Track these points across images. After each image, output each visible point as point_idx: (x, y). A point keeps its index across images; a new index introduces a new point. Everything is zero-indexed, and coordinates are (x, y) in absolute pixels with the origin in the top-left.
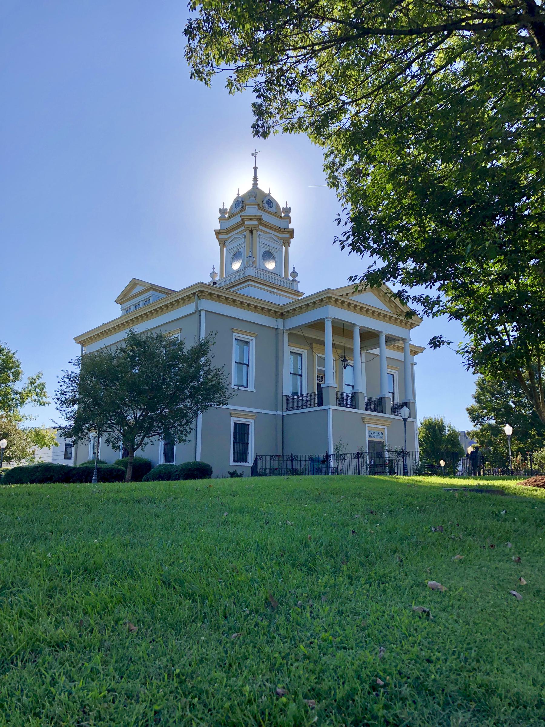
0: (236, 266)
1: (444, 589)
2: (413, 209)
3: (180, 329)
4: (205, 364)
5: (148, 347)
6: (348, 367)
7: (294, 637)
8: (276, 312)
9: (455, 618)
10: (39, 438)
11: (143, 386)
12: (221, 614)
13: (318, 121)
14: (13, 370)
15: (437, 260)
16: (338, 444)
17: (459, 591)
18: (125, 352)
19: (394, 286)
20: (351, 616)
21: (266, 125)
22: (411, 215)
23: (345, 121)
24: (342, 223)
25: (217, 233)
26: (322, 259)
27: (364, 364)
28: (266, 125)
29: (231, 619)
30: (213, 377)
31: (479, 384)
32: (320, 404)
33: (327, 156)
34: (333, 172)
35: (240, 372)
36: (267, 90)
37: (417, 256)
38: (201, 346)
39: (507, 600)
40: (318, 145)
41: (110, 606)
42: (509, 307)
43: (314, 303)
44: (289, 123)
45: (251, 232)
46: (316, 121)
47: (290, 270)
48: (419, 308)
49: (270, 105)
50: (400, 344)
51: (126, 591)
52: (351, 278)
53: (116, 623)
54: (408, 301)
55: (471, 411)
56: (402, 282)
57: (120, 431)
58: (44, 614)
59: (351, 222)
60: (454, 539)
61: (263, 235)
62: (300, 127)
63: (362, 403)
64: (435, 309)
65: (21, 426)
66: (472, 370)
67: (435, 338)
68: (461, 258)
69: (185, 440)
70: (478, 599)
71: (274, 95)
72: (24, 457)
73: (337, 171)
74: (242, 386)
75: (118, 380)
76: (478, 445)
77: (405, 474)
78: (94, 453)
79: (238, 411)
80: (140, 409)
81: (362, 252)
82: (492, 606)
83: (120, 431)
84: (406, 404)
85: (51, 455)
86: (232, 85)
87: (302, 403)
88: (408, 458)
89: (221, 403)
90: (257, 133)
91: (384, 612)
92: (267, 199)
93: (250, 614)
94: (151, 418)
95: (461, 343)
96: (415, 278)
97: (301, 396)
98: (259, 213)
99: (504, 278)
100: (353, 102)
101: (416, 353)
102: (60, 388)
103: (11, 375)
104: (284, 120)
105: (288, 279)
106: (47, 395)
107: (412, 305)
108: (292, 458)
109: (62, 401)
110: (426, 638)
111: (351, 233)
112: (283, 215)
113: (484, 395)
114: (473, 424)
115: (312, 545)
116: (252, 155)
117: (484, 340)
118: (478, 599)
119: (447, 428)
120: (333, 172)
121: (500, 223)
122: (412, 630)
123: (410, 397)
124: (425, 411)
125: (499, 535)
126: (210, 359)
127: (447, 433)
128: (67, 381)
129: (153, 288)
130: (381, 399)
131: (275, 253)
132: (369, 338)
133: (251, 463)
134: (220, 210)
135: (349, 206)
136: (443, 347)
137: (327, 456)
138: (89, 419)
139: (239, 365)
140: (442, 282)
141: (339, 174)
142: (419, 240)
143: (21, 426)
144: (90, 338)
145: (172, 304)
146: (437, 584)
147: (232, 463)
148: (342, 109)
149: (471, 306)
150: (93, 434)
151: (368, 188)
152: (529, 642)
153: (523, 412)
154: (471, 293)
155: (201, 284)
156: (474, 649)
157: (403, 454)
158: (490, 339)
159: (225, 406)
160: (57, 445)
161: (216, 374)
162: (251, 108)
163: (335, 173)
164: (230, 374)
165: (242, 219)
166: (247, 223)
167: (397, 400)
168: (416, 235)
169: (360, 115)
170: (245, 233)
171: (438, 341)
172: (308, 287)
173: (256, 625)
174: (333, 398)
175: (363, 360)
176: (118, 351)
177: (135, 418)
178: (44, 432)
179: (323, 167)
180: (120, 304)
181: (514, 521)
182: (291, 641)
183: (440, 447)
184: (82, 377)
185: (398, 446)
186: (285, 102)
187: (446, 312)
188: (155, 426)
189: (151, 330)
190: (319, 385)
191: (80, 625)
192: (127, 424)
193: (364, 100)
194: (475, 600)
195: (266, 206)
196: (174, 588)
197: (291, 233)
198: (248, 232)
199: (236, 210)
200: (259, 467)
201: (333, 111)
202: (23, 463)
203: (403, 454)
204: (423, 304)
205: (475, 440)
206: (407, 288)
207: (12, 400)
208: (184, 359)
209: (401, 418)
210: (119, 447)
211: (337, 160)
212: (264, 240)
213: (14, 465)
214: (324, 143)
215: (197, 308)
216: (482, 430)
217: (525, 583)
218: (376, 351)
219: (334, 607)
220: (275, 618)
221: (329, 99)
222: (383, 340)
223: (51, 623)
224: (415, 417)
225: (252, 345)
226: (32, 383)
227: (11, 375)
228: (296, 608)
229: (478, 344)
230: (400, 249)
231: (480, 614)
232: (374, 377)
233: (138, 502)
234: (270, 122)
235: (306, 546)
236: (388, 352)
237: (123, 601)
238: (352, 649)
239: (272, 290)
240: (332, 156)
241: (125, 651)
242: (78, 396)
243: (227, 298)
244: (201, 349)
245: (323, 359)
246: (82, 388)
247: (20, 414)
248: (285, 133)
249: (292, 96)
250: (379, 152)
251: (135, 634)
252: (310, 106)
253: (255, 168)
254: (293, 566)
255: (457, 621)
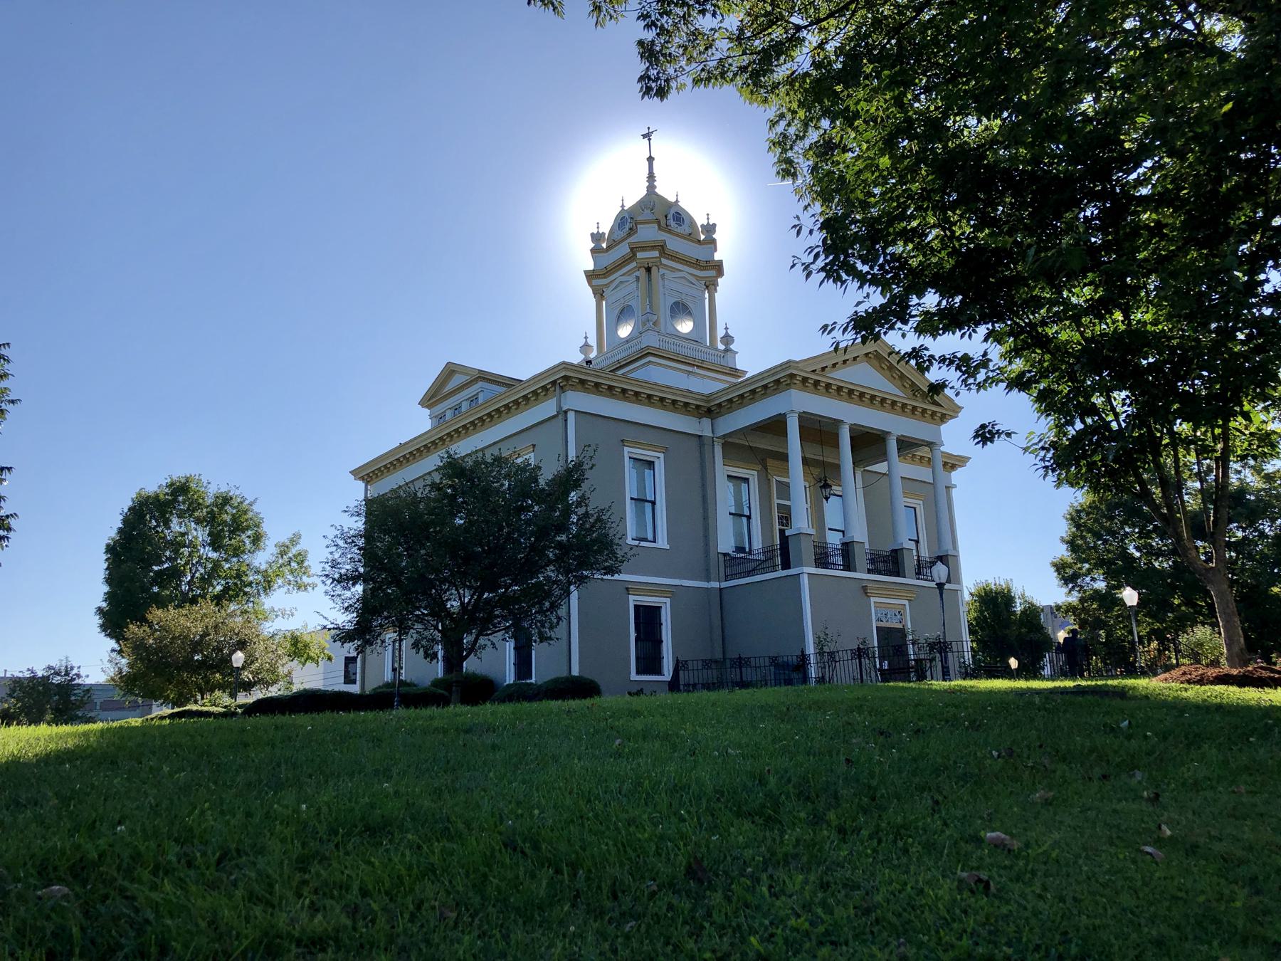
0: (625, 331)
1: (1016, 845)
2: (929, 199)
3: (533, 445)
4: (579, 504)
5: (479, 479)
6: (832, 499)
7: (739, 926)
8: (698, 407)
9: (1038, 891)
10: (298, 648)
11: (469, 537)
12: (605, 890)
13: (754, 62)
14: (249, 533)
15: (979, 290)
16: (822, 635)
17: (1044, 848)
18: (439, 489)
19: (901, 339)
20: (843, 892)
21: (663, 77)
22: (926, 210)
23: (802, 60)
24: (805, 231)
25: (590, 276)
26: (773, 302)
27: (860, 491)
28: (663, 77)
29: (627, 901)
30: (593, 526)
31: (1072, 519)
32: (786, 565)
33: (773, 124)
34: (784, 151)
35: (640, 515)
36: (661, 15)
37: (944, 285)
38: (569, 472)
39: (1134, 861)
40: (756, 104)
41: (407, 880)
42: (1113, 359)
43: (765, 387)
44: (703, 70)
45: (648, 270)
46: (750, 63)
47: (720, 333)
48: (951, 375)
49: (668, 42)
50: (923, 452)
51: (435, 859)
52: (825, 327)
53: (419, 907)
54: (931, 364)
55: (1060, 567)
56: (920, 330)
57: (436, 628)
58: (290, 894)
59: (821, 229)
60: (1032, 768)
61: (669, 275)
62: (723, 75)
63: (861, 559)
64: (981, 376)
65: (268, 628)
66: (1051, 478)
67: (983, 426)
68: (1019, 280)
69: (550, 638)
70: (1081, 861)
71: (675, 24)
72: (274, 682)
73: (791, 148)
74: (646, 540)
75: (428, 539)
76: (1076, 627)
77: (946, 675)
78: (394, 670)
79: (641, 584)
80: (470, 588)
81: (843, 282)
82: (1108, 872)
83: (436, 628)
84: (942, 559)
85: (322, 677)
86: (600, 11)
87: (753, 565)
88: (950, 654)
89: (611, 570)
90: (647, 91)
91: (906, 884)
92: (672, 212)
93: (660, 890)
94: (488, 601)
95: (1031, 433)
96: (940, 321)
97: (750, 552)
98: (663, 236)
99: (1098, 309)
100: (811, 24)
101: (953, 467)
102: (330, 557)
103: (247, 541)
104: (694, 65)
105: (717, 349)
106: (312, 571)
107: (935, 374)
108: (741, 662)
109: (334, 580)
110: (984, 925)
111: (820, 249)
112: (703, 237)
113: (1083, 537)
114: (1065, 590)
115: (772, 781)
116: (644, 136)
117: (1072, 424)
118: (1081, 861)
119: (1018, 601)
120: (784, 151)
121: (1088, 213)
122: (958, 911)
123: (947, 547)
124: (976, 573)
125: (1118, 760)
126: (587, 495)
127: (1018, 608)
128: (341, 543)
129: (483, 377)
130: (895, 551)
131: (690, 305)
132: (869, 444)
133: (667, 674)
134: (592, 235)
135: (817, 207)
136: (999, 442)
137: (804, 658)
138: (383, 608)
139: (640, 505)
140: (990, 326)
141: (797, 154)
142: (943, 254)
143: (268, 628)
144: (379, 469)
145: (516, 402)
146: (1003, 836)
147: (634, 676)
148: (795, 40)
149: (1046, 364)
150: (390, 635)
151: (848, 167)
152: (1177, 927)
153: (1156, 564)
154: (1044, 342)
155: (565, 365)
156: (1075, 940)
157: (941, 647)
158: (1083, 422)
159: (616, 577)
160: (330, 659)
161: (598, 520)
162: (636, 50)
163: (790, 154)
164: (623, 519)
165: (632, 249)
166: (639, 255)
167: (925, 553)
168: (936, 244)
169: (828, 47)
170: (637, 274)
171: (990, 432)
172: (753, 360)
173: (670, 907)
174: (808, 552)
175: (860, 484)
176: (428, 488)
177: (462, 603)
178: (307, 638)
179: (767, 144)
180: (429, 407)
181: (1146, 737)
182: (734, 932)
183: (1005, 628)
184: (368, 535)
185: (931, 633)
186: (695, 34)
187: (1002, 381)
188: (497, 616)
189: (482, 450)
190: (782, 532)
191: (353, 911)
192: (449, 614)
193: (832, 21)
194: (1075, 863)
195: (673, 224)
196: (523, 852)
197: (718, 268)
198: (643, 270)
199: (621, 234)
200: (682, 682)
201: (781, 43)
202: (273, 692)
203: (941, 647)
204: (958, 368)
205: (1071, 619)
206: (927, 341)
207: (250, 584)
208: (541, 497)
209: (933, 585)
210: (435, 656)
211: (792, 130)
212: (672, 282)
213: (258, 694)
214: (765, 101)
215: (560, 408)
216: (1082, 600)
217: (1169, 833)
218: (881, 467)
219: (812, 878)
220: (704, 897)
221: (771, 23)
222: (892, 445)
223: (302, 908)
224: (959, 582)
225: (660, 466)
226: (282, 554)
227: (247, 541)
228: (743, 879)
229: (1060, 428)
230: (912, 271)
231: (1085, 886)
232: (879, 514)
233: (467, 731)
234: (671, 71)
235: (762, 782)
236: (902, 468)
237: (430, 871)
238: (847, 944)
239: (690, 369)
240: (783, 123)
241: (433, 950)
242: (361, 570)
243: (611, 388)
244: (571, 477)
245: (787, 485)
246: (368, 554)
247: (266, 607)
248: (696, 88)
249: (705, 23)
250: (863, 104)
251: (451, 923)
252: (739, 38)
253: (650, 159)
254: (739, 814)
255: (1040, 897)
